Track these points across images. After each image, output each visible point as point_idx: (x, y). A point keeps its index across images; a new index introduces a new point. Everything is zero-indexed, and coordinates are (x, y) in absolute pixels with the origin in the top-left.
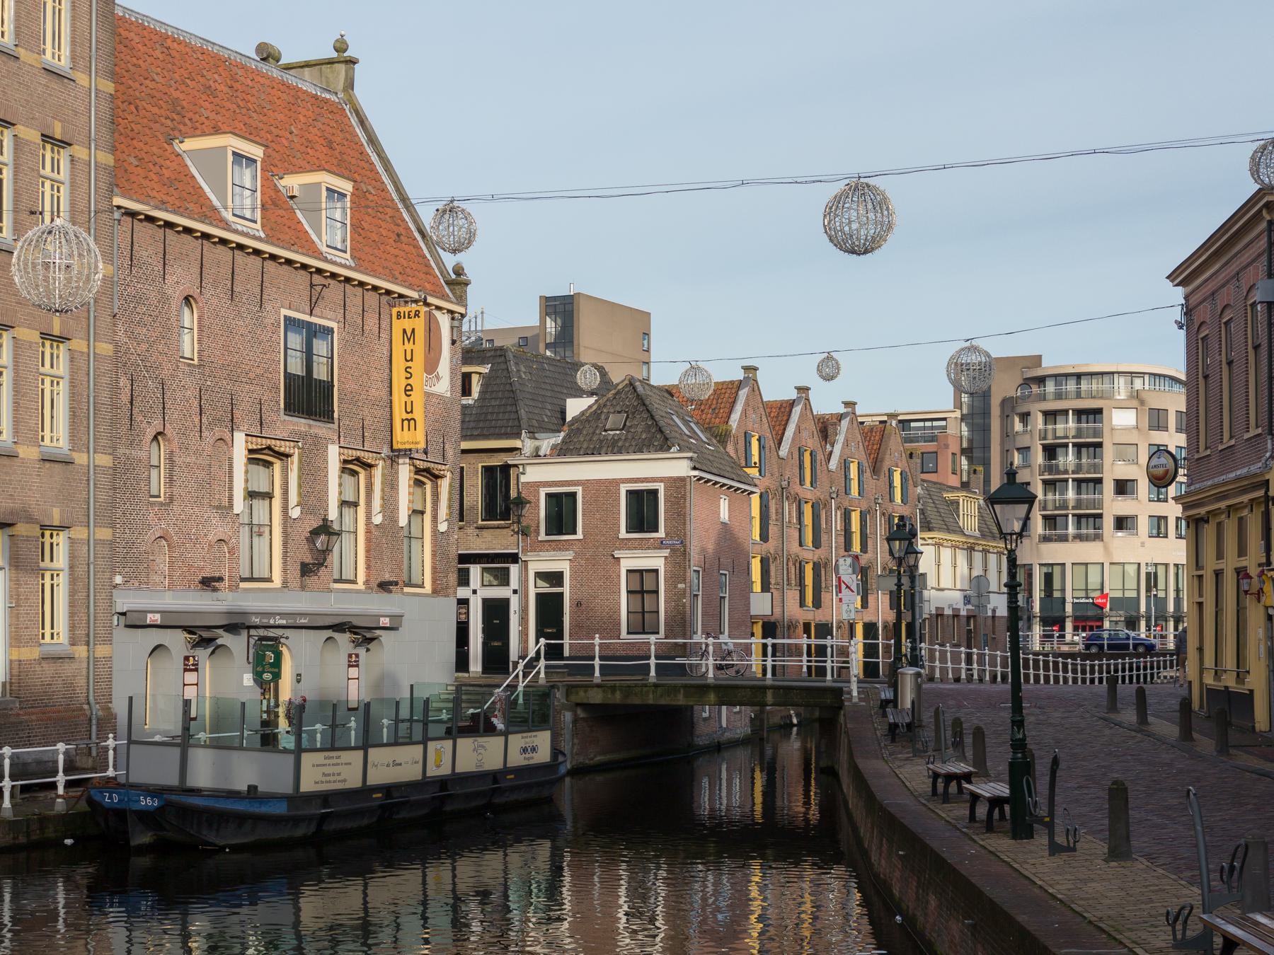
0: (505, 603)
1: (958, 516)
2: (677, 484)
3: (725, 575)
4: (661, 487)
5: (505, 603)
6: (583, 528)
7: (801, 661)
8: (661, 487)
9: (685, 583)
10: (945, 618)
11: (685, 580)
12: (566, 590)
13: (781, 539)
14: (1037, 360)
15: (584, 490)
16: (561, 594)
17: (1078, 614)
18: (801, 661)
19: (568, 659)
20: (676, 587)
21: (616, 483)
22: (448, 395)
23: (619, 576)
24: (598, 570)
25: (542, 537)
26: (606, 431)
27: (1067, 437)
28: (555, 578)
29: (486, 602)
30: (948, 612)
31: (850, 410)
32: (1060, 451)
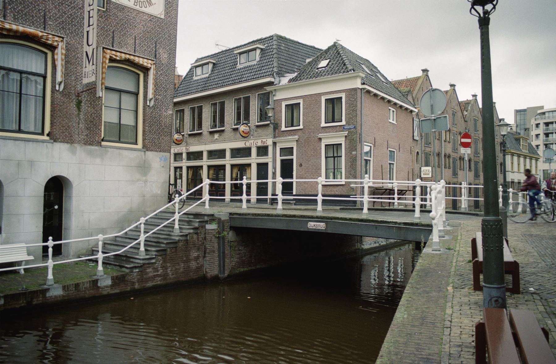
0: (266, 164)
1: (520, 145)
2: (352, 92)
3: (394, 152)
4: (343, 95)
5: (266, 164)
6: (303, 122)
7: (394, 199)
8: (343, 95)
9: (356, 151)
10: (515, 184)
11: (356, 149)
12: (294, 157)
13: (441, 146)
14: (542, 107)
15: (304, 101)
16: (292, 160)
17: (413, 213)
18: (394, 199)
19: (294, 195)
20: (351, 154)
21: (320, 95)
22: (163, 17)
23: (321, 148)
24: (310, 145)
25: (283, 128)
26: (318, 69)
27: (553, 130)
28: (289, 151)
29: (259, 165)
30: (516, 181)
31: (474, 98)
32: (550, 135)
